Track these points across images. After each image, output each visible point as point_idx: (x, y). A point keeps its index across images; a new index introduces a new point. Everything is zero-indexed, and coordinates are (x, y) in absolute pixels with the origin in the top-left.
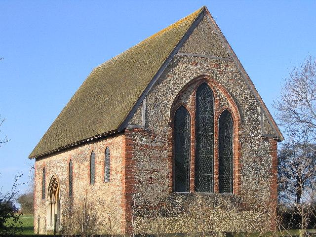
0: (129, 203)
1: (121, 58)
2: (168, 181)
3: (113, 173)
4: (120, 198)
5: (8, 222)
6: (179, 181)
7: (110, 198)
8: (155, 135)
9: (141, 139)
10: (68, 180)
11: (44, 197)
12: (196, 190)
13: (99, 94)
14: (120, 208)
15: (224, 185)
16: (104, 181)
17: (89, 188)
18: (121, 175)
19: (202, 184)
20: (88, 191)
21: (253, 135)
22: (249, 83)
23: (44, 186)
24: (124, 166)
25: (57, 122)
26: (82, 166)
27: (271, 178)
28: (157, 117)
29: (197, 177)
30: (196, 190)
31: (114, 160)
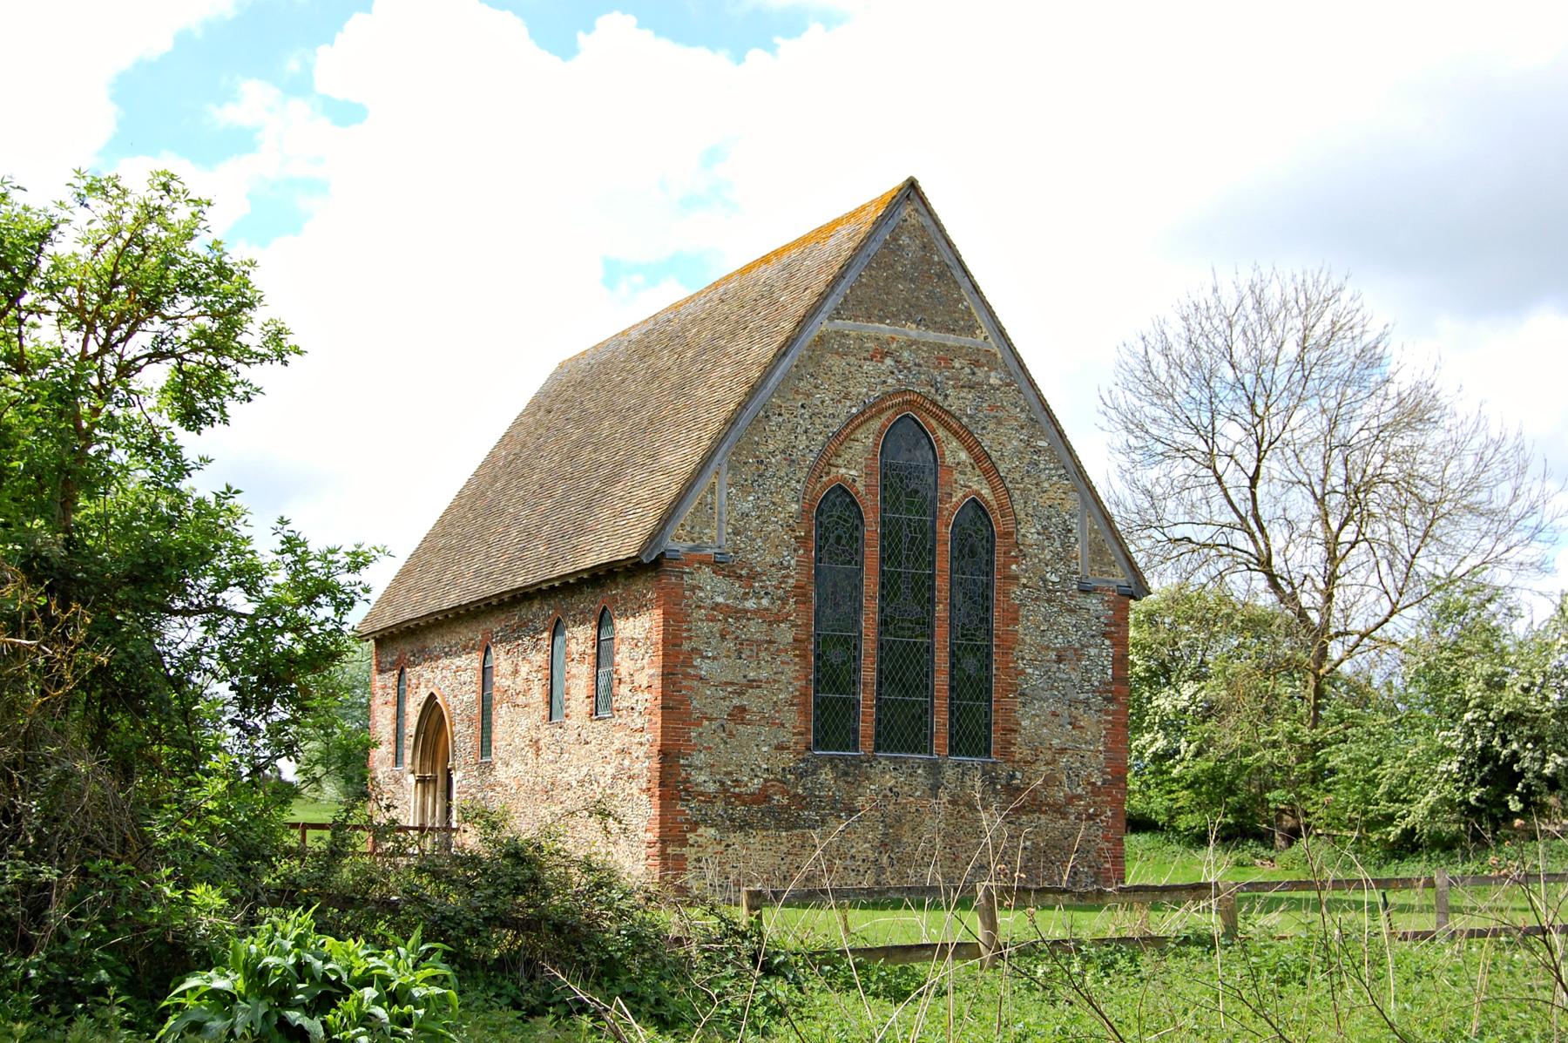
0: (671, 783)
1: (647, 334)
2: (793, 719)
3: (624, 690)
4: (645, 765)
5: (581, 35)
6: (830, 724)
7: (610, 770)
8: (753, 576)
9: (712, 588)
10: (477, 710)
11: (398, 760)
12: (878, 748)
13: (579, 445)
14: (644, 797)
15: (972, 737)
16: (594, 713)
17: (545, 735)
18: (647, 696)
19: (902, 733)
20: (541, 743)
21: (1054, 578)
22: (1088, 902)
23: (400, 715)
24: (657, 670)
25: (445, 525)
26: (524, 669)
27: (1107, 713)
28: (766, 525)
29: (878, 899)
30: (878, 748)
31: (624, 649)
